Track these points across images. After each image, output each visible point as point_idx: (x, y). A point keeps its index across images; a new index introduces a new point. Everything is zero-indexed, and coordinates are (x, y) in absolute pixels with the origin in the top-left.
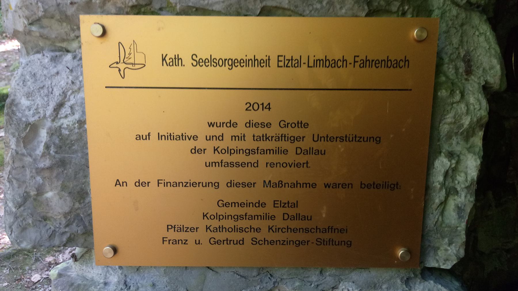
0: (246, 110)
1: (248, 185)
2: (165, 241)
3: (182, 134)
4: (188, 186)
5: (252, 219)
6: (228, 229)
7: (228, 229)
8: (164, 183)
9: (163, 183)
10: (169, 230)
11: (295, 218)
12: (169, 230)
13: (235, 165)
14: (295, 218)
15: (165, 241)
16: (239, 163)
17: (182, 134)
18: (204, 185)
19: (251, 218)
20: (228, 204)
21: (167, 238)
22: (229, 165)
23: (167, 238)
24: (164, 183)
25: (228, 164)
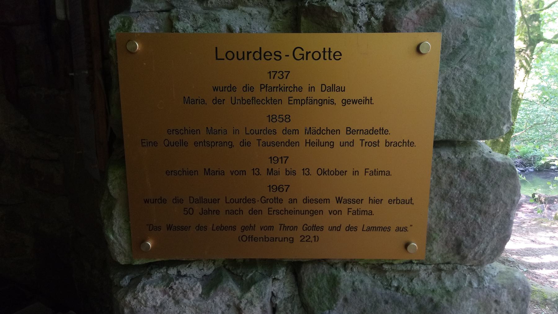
0: (301, 241)
1: (357, 201)
2: (350, 212)
3: (358, 209)
4: (273, 72)
5: (292, 203)
6: (234, 202)
7: (234, 202)
8: (147, 142)
9: (146, 142)
10: (258, 141)
11: (199, 201)
12: (258, 141)
13: (352, 201)
14: (199, 201)
15: (350, 212)
16: (355, 200)
17: (358, 209)
18: (281, 240)
19: (291, 202)
20: (358, 200)
21: (292, 97)
22: (347, 201)
23: (292, 97)
24: (147, 142)
25: (346, 201)
